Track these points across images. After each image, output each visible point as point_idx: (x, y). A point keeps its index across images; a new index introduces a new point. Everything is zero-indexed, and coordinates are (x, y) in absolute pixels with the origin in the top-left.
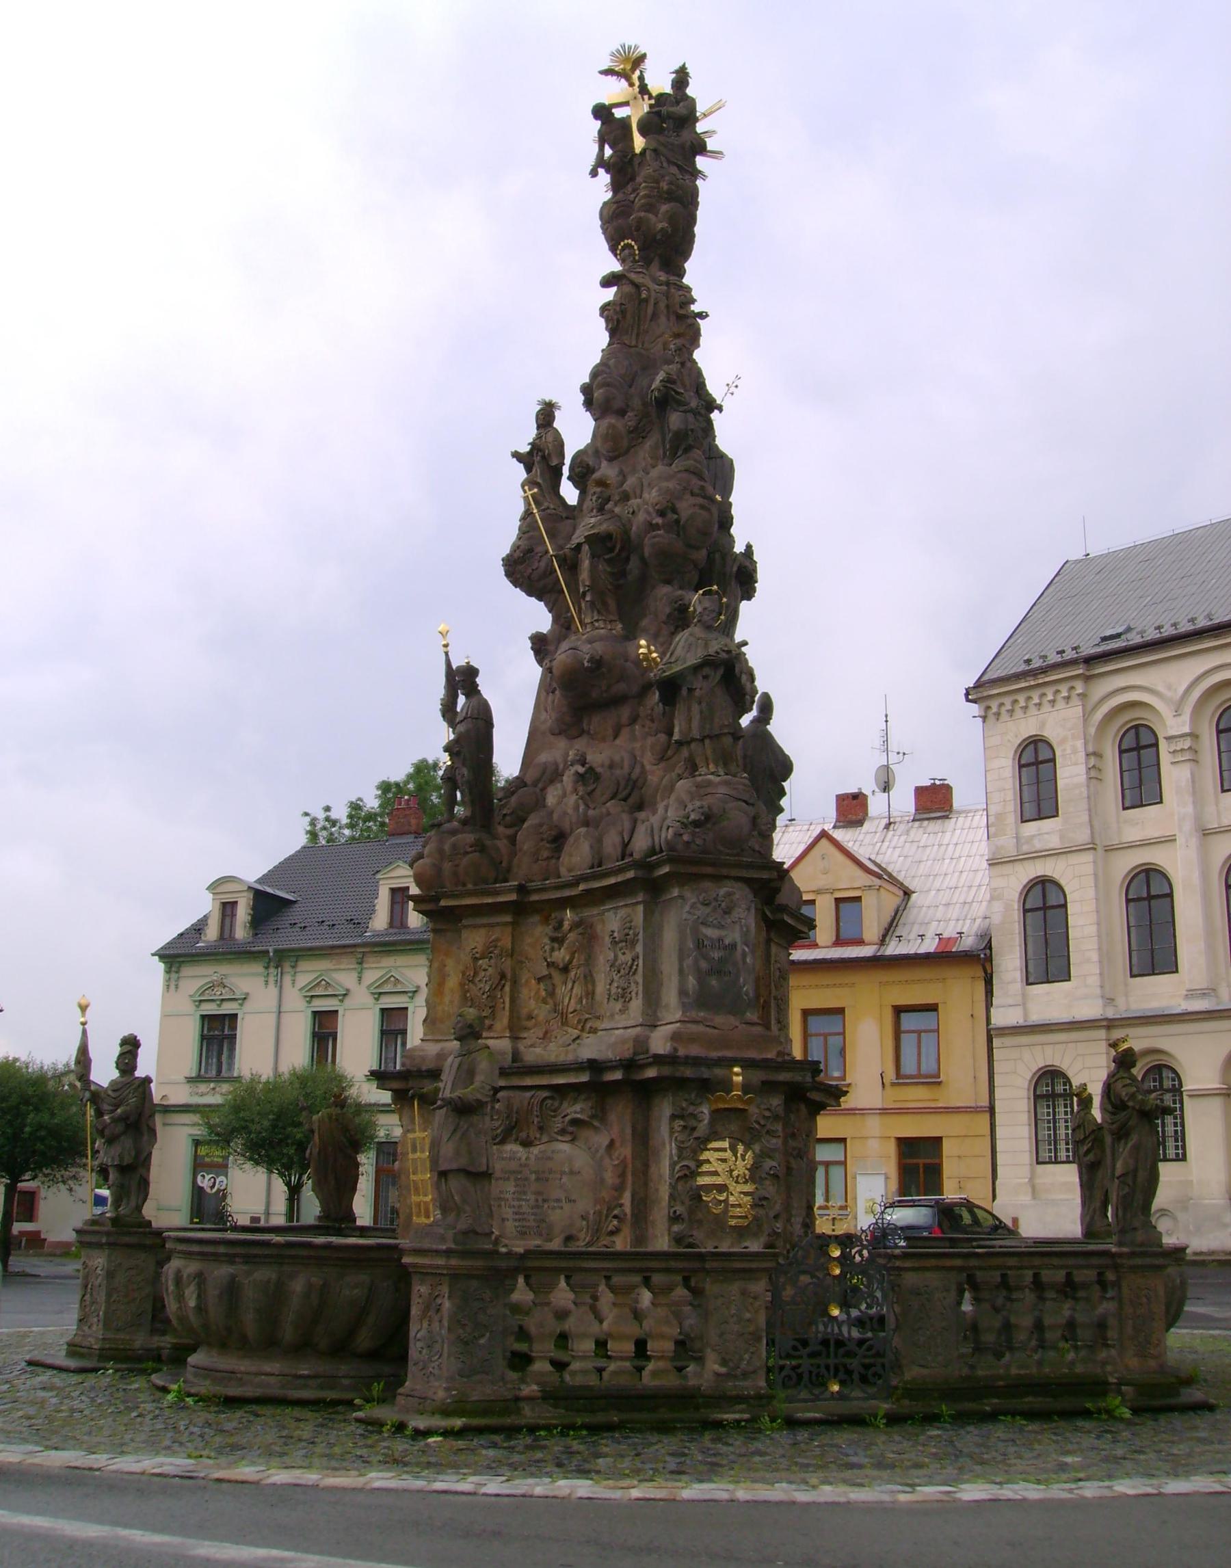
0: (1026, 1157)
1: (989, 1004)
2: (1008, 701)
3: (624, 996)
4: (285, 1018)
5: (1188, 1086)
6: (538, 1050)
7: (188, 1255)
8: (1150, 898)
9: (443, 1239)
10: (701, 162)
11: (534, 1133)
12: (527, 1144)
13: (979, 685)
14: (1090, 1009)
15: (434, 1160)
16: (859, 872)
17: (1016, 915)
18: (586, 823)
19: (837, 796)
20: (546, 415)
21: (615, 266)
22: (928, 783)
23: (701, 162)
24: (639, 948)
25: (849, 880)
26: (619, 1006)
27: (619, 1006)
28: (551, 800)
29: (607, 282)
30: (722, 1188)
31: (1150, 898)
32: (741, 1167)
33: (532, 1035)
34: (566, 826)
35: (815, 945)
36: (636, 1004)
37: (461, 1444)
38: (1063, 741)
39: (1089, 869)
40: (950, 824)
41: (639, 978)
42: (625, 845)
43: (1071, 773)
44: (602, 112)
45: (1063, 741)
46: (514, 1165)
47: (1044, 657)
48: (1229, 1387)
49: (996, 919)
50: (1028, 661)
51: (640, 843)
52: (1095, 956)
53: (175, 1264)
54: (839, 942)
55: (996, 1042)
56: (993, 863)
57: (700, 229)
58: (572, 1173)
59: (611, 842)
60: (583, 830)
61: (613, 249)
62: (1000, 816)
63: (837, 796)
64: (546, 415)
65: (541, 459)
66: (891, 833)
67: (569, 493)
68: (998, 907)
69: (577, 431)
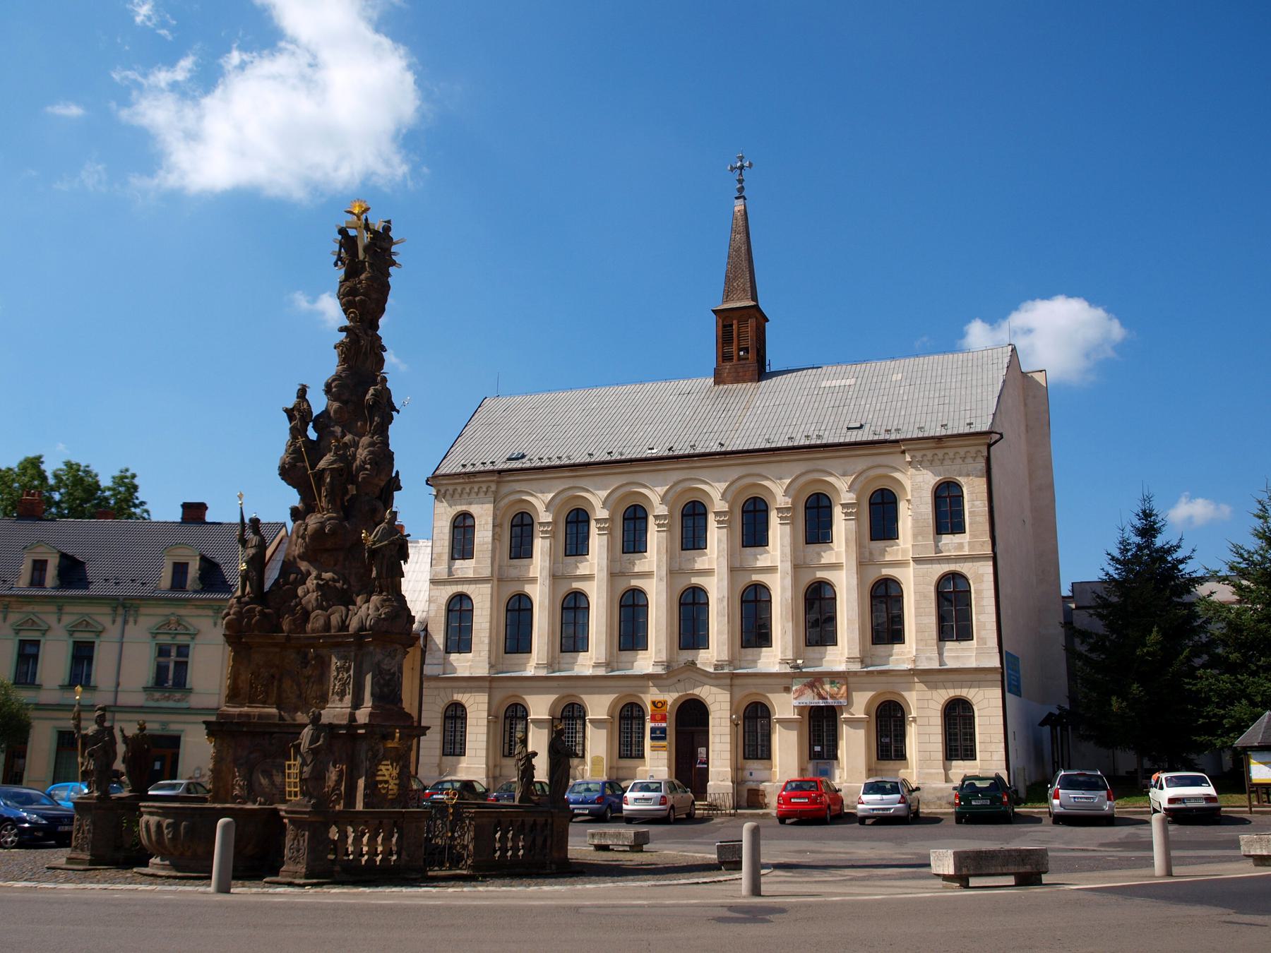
0: (438, 752)
1: (423, 663)
2: (451, 488)
3: (342, 694)
4: (112, 685)
5: (532, 716)
7: (151, 814)
8: (519, 610)
9: (306, 806)
10: (392, 270)
13: (435, 477)
14: (483, 671)
17: (443, 613)
20: (302, 392)
21: (347, 323)
23: (392, 270)
24: (352, 672)
28: (300, 592)
29: (341, 330)
30: (386, 782)
31: (519, 610)
32: (395, 773)
37: (318, 889)
38: (481, 516)
39: (489, 591)
42: (343, 622)
43: (483, 535)
44: (343, 232)
45: (481, 516)
47: (473, 465)
48: (1260, 772)
49: (432, 614)
50: (464, 466)
51: (354, 624)
52: (487, 641)
53: (145, 817)
55: (425, 685)
56: (434, 582)
59: (335, 619)
60: (319, 612)
61: (345, 311)
62: (440, 555)
64: (302, 392)
65: (299, 415)
67: (312, 435)
68: (433, 607)
69: (319, 403)
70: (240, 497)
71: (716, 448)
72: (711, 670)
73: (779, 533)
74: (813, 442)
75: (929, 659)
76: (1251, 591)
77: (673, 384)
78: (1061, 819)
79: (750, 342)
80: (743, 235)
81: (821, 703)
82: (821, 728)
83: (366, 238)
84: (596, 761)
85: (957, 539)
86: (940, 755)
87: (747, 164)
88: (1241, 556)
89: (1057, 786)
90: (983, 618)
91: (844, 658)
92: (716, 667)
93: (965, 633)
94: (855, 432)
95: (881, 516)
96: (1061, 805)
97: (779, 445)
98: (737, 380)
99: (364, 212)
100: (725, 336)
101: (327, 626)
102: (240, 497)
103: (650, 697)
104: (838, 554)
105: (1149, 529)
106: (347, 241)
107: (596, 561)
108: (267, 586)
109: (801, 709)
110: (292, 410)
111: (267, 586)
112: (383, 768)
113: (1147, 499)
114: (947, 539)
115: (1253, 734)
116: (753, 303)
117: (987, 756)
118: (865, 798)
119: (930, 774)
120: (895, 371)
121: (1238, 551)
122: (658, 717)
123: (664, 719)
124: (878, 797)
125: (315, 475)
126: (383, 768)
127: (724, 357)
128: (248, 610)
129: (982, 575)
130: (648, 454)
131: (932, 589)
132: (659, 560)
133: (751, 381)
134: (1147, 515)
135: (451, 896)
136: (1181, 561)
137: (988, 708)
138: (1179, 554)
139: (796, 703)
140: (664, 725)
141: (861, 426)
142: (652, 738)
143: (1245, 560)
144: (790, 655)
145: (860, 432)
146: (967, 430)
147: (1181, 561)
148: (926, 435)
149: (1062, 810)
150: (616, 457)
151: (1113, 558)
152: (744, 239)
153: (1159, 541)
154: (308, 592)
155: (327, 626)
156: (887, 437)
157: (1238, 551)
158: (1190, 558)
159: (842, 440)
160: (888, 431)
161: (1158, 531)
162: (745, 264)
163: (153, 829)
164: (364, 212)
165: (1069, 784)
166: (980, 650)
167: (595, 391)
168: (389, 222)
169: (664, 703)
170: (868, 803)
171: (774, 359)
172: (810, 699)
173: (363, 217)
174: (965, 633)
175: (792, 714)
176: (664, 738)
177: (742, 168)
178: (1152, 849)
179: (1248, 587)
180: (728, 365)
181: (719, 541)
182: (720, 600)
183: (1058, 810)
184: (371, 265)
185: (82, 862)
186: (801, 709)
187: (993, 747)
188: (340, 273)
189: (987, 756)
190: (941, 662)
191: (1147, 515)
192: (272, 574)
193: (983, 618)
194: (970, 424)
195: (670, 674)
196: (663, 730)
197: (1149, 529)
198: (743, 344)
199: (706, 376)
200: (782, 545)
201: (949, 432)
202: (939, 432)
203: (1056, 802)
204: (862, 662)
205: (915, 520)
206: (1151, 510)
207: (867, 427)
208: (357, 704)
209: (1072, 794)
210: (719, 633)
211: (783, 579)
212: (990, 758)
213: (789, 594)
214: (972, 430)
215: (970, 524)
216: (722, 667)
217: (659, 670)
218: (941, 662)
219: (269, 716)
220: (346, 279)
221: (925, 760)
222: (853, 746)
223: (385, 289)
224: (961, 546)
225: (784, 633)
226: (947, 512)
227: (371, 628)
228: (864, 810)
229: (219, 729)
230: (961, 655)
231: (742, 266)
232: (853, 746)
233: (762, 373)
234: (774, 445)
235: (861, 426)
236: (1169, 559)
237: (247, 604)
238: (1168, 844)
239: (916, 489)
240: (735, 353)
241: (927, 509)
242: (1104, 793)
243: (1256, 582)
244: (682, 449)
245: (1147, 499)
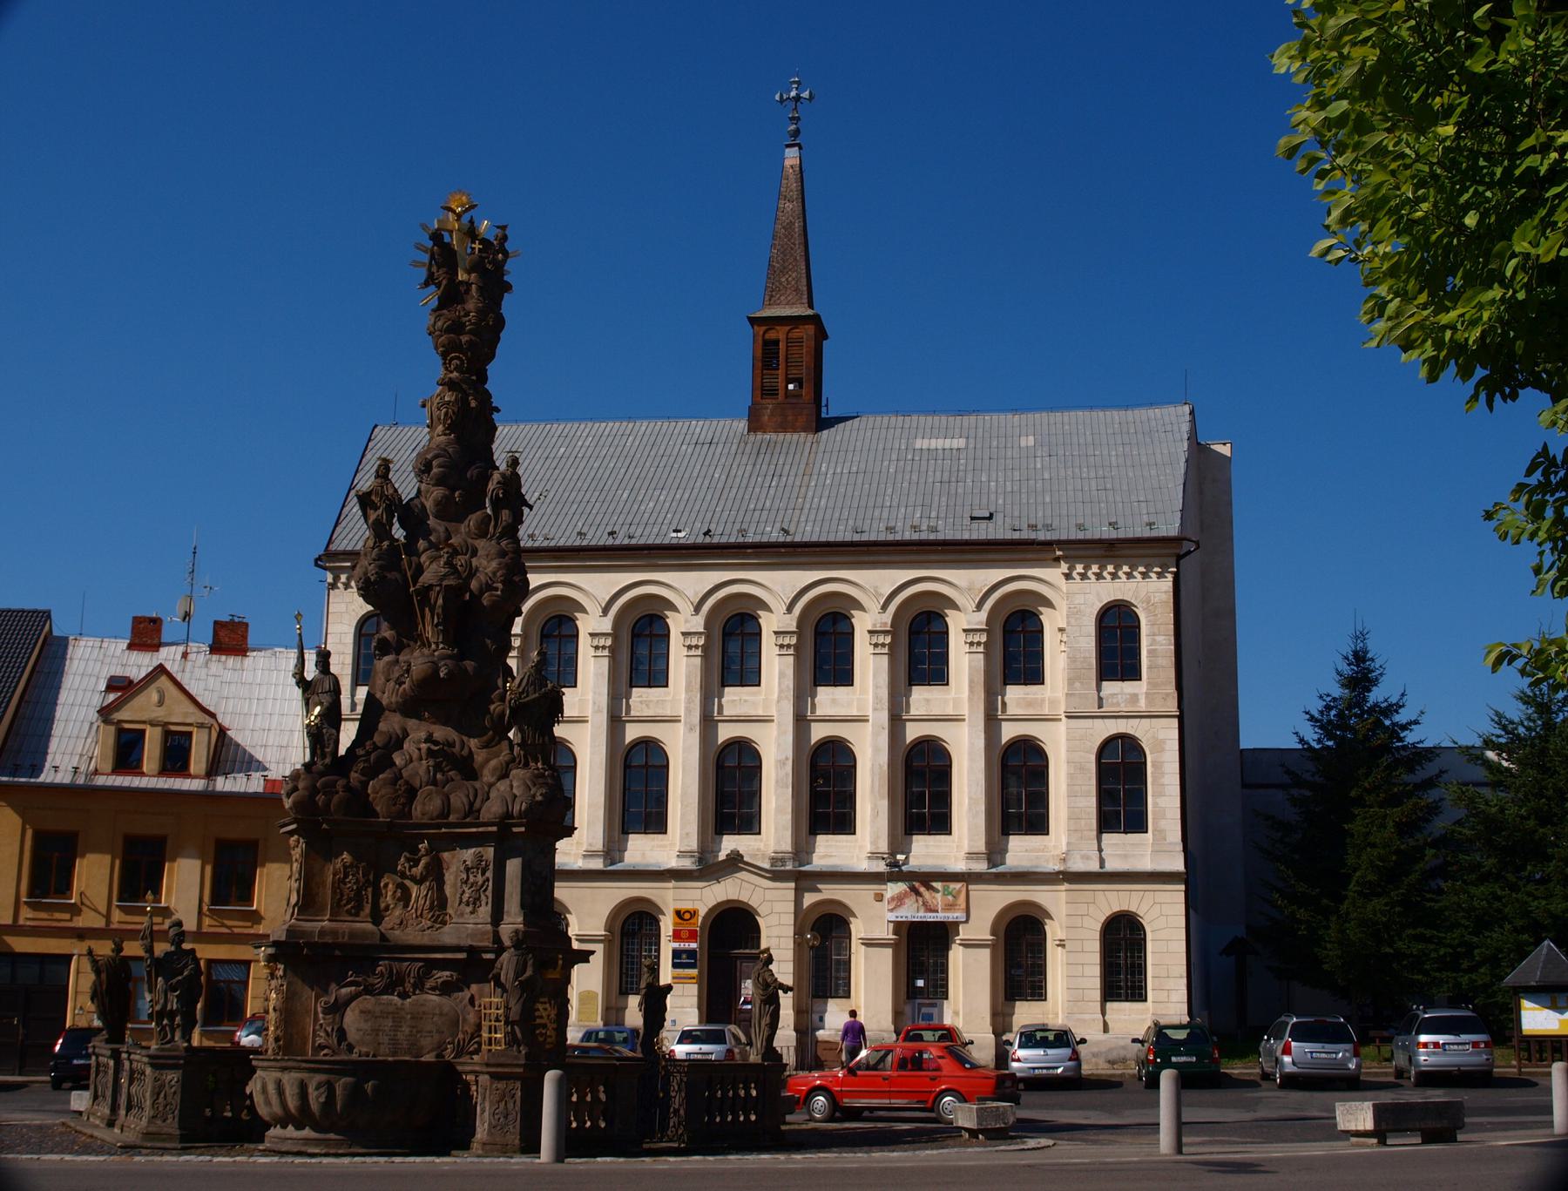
3: (476, 902)
6: (397, 932)
11: (408, 987)
12: (404, 995)
15: (507, 1017)
16: (192, 709)
18: (434, 783)
19: (135, 618)
22: (227, 619)
24: (489, 874)
25: (179, 713)
26: (470, 909)
27: (470, 909)
28: (398, 759)
30: (544, 1026)
33: (389, 921)
34: (417, 783)
35: (142, 774)
36: (485, 911)
40: (248, 661)
41: (489, 893)
42: (471, 804)
44: (436, 237)
46: (391, 1009)
48: (1537, 1019)
54: (164, 771)
57: (500, 349)
58: (441, 1014)
59: (458, 800)
63: (135, 618)
66: (189, 664)
67: (398, 533)
70: (298, 617)
71: (776, 536)
72: (767, 866)
73: (871, 666)
74: (924, 536)
75: (1086, 858)
76: (1512, 775)
77: (681, 426)
78: (1292, 1082)
79: (805, 372)
80: (796, 205)
81: (930, 917)
82: (922, 951)
83: (466, 251)
84: (586, 998)
85: (1128, 687)
86: (1097, 995)
87: (806, 94)
88: (1504, 728)
89: (1287, 1038)
90: (1162, 802)
91: (962, 854)
92: (774, 861)
93: (1136, 822)
94: (983, 524)
95: (1016, 648)
96: (1294, 1063)
97: (873, 538)
98: (783, 427)
99: (467, 210)
100: (768, 356)
101: (446, 810)
102: (298, 617)
103: (670, 899)
104: (957, 702)
105: (1360, 676)
106: (442, 255)
107: (590, 697)
108: (342, 751)
109: (898, 926)
110: (369, 494)
111: (342, 751)
112: (540, 1007)
113: (1361, 636)
114: (1109, 687)
115: (1532, 968)
116: (810, 312)
117: (1163, 996)
118: (1021, 1053)
119: (1084, 1021)
120: (1025, 433)
121: (1501, 720)
122: (684, 935)
123: (692, 936)
124: (1041, 1052)
125: (418, 592)
126: (540, 1007)
127: (765, 391)
128: (325, 785)
129: (1163, 741)
130: (672, 537)
131: (1093, 758)
132: (689, 701)
133: (805, 430)
134: (1360, 657)
135: (899, 1160)
136: (1404, 727)
137: (1166, 923)
138: (1402, 717)
139: (892, 916)
140: (694, 945)
141: (991, 517)
142: (675, 966)
143: (1507, 732)
144: (884, 847)
145: (991, 524)
146: (1147, 533)
147: (1404, 727)
148: (1089, 536)
149: (1294, 1069)
150: (622, 540)
151: (1312, 719)
152: (798, 210)
153: (1376, 696)
154: (412, 756)
155: (446, 810)
156: (1033, 536)
157: (1501, 720)
158: (1416, 722)
159: (966, 536)
160: (1033, 527)
161: (1375, 682)
162: (799, 251)
163: (271, 1088)
164: (467, 210)
165: (1301, 1034)
166: (1160, 843)
167: (557, 428)
168: (504, 228)
169: (694, 914)
170: (1026, 1060)
171: (834, 398)
172: (911, 912)
173: (465, 219)
174: (1136, 822)
175: (886, 933)
176: (692, 966)
177: (798, 98)
178: (1551, 1113)
179: (1507, 769)
180: (769, 404)
181: (782, 675)
182: (781, 763)
183: (1290, 1069)
184: (480, 289)
185: (170, 1137)
186: (898, 926)
187: (1171, 984)
188: (431, 297)
189: (1163, 996)
190: (1102, 862)
191: (1360, 657)
192: (348, 734)
193: (1162, 802)
194: (1150, 524)
195: (708, 868)
196: (691, 953)
197: (1360, 676)
198: (794, 372)
199: (733, 416)
200: (876, 687)
201: (1121, 535)
202: (1107, 533)
203: (1287, 1059)
204: (989, 860)
205: (1072, 659)
206: (1366, 652)
207: (999, 518)
208: (497, 916)
209: (1308, 1047)
210: (779, 810)
211: (875, 735)
212: (1168, 994)
213: (884, 758)
214: (1154, 534)
215: (1149, 668)
216: (783, 861)
217: (688, 864)
218: (1102, 862)
219: (364, 934)
220: (441, 306)
221: (1076, 1000)
222: (969, 979)
223: (500, 323)
224: (1134, 698)
225: (875, 814)
226: (1116, 644)
227: (521, 815)
228: (1021, 1070)
229: (289, 953)
230: (1124, 851)
231: (795, 254)
232: (969, 979)
233: (823, 424)
234: (865, 538)
235: (991, 517)
236: (1387, 723)
237: (322, 774)
238: (1180, 1127)
239: (1070, 607)
240: (781, 385)
241: (1088, 643)
242: (1349, 1046)
243: (1519, 762)
244: (726, 533)
245: (1361, 636)
